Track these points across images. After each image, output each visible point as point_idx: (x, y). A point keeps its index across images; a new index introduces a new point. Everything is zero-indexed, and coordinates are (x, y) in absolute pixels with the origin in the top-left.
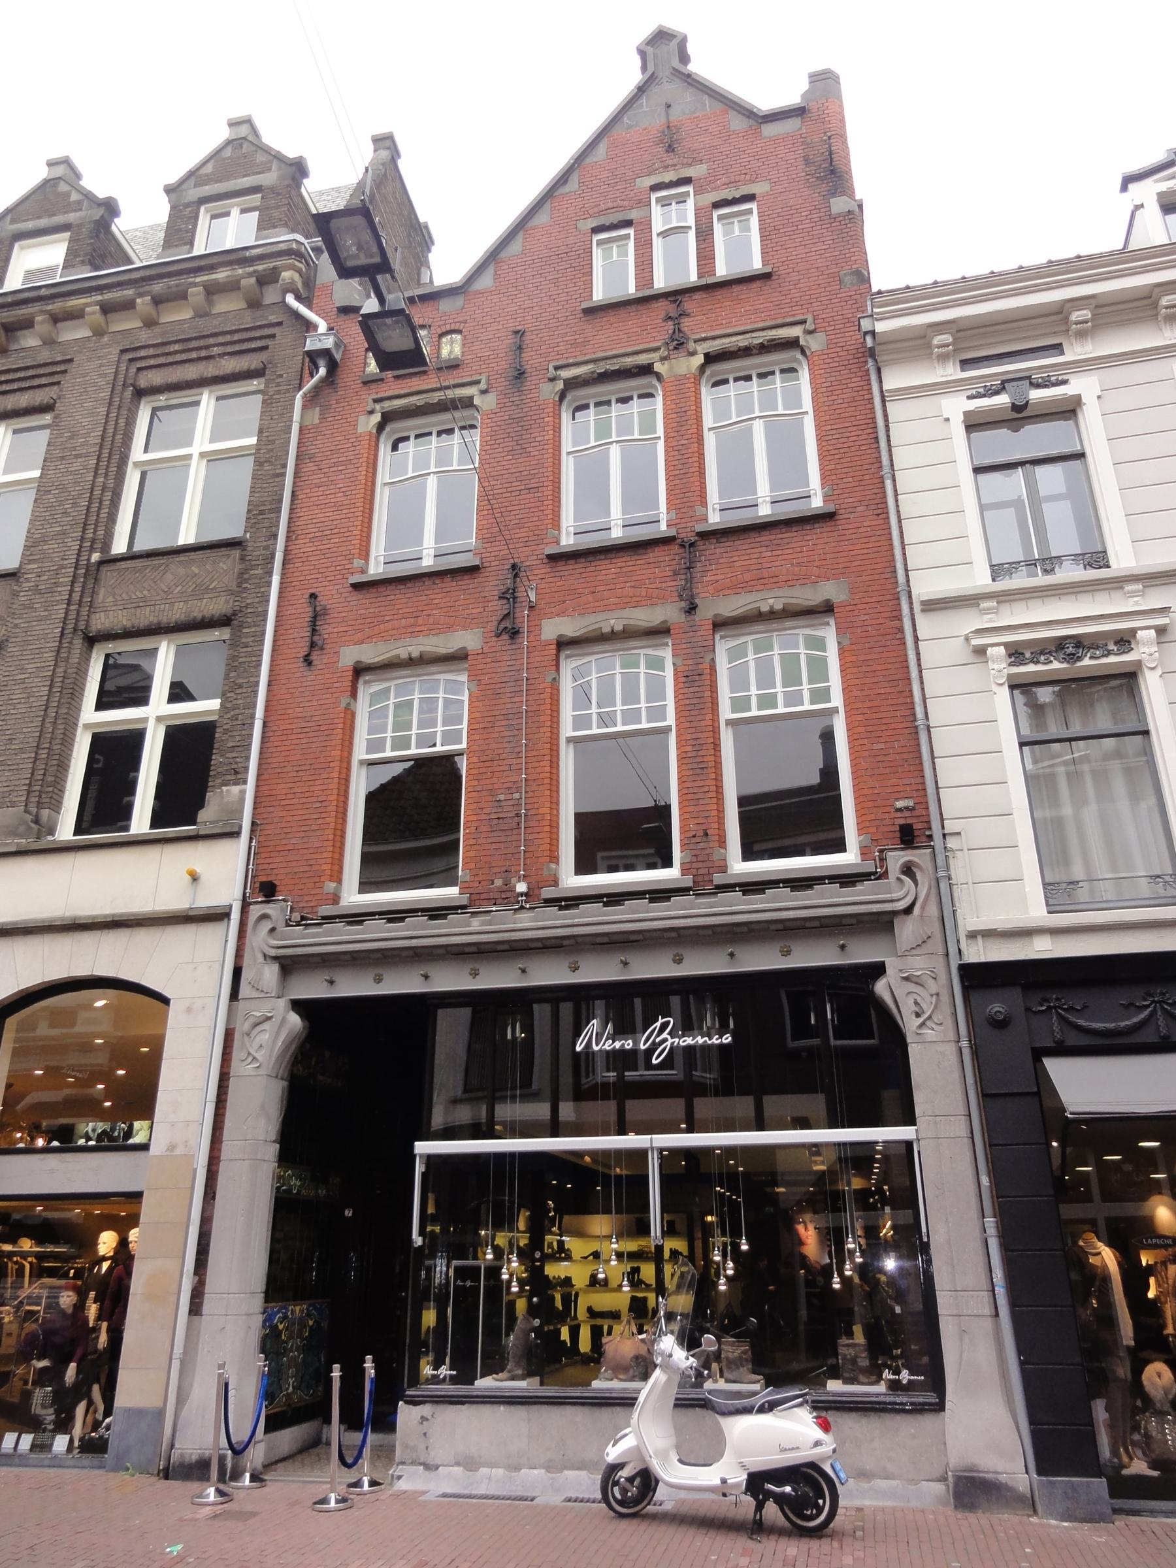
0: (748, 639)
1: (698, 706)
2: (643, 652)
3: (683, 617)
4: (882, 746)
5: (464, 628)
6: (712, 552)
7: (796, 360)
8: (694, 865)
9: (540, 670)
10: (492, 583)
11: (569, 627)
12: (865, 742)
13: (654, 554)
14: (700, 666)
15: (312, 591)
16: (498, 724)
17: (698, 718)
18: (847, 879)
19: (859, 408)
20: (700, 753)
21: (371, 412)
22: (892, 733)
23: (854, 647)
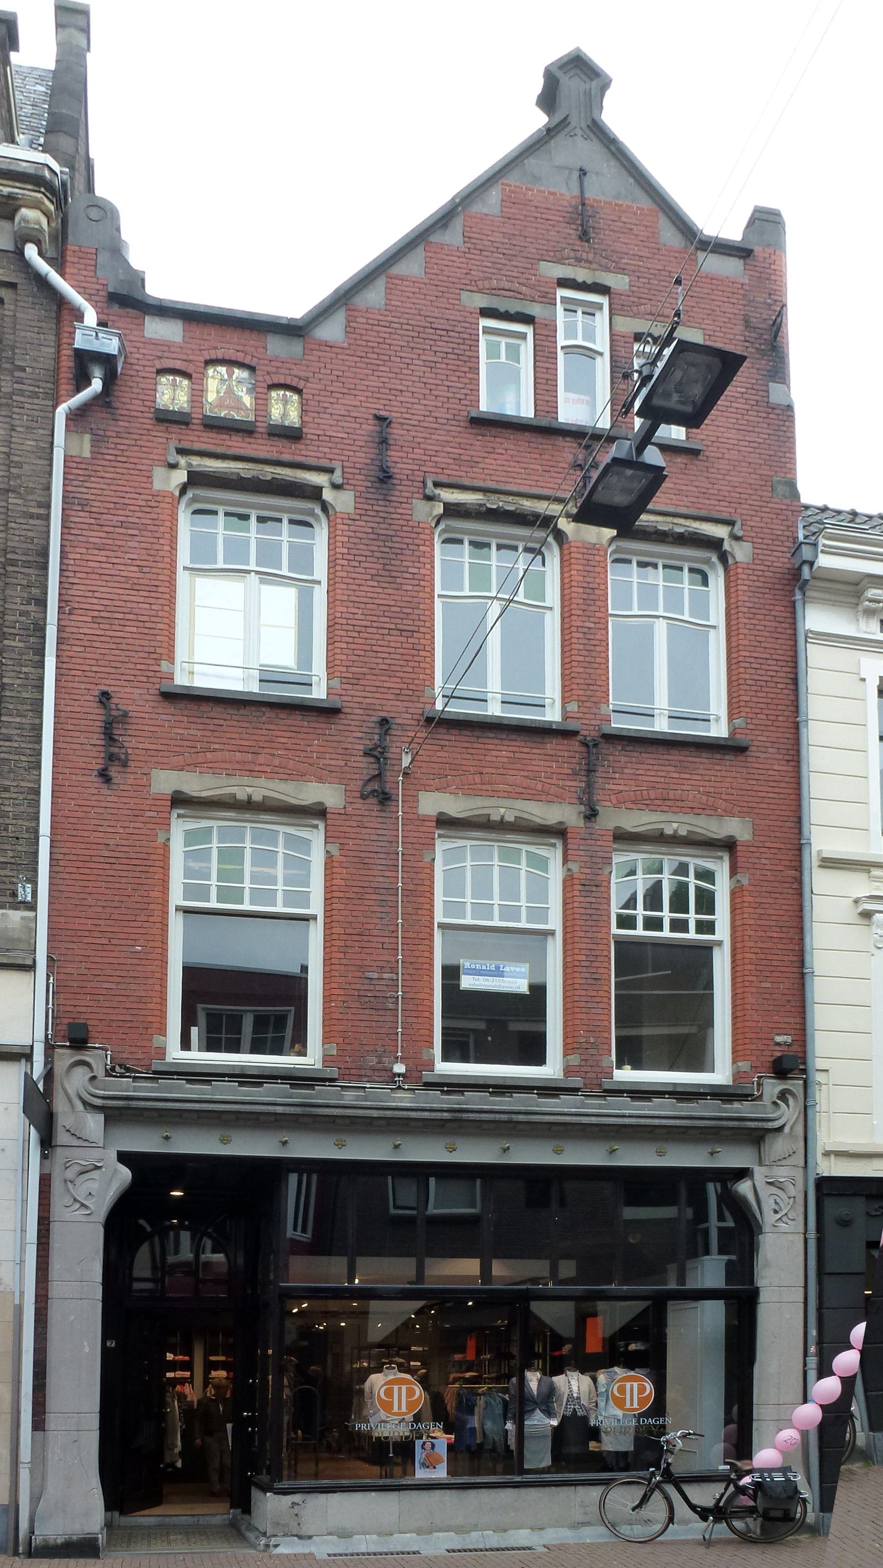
0: (214, 824)
1: (593, 917)
2: (526, 848)
3: (581, 823)
4: (769, 985)
5: (320, 780)
6: (617, 758)
7: (312, 513)
8: (583, 1069)
9: (418, 847)
10: (355, 734)
11: (454, 806)
12: (754, 978)
13: (552, 746)
14: (598, 878)
15: (105, 688)
16: (367, 896)
17: (594, 929)
18: (548, 1090)
19: (780, 641)
20: (595, 964)
21: (173, 466)
22: (779, 974)
23: (752, 888)
